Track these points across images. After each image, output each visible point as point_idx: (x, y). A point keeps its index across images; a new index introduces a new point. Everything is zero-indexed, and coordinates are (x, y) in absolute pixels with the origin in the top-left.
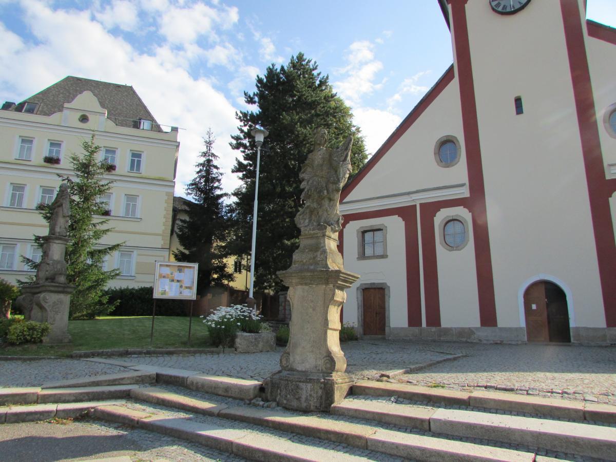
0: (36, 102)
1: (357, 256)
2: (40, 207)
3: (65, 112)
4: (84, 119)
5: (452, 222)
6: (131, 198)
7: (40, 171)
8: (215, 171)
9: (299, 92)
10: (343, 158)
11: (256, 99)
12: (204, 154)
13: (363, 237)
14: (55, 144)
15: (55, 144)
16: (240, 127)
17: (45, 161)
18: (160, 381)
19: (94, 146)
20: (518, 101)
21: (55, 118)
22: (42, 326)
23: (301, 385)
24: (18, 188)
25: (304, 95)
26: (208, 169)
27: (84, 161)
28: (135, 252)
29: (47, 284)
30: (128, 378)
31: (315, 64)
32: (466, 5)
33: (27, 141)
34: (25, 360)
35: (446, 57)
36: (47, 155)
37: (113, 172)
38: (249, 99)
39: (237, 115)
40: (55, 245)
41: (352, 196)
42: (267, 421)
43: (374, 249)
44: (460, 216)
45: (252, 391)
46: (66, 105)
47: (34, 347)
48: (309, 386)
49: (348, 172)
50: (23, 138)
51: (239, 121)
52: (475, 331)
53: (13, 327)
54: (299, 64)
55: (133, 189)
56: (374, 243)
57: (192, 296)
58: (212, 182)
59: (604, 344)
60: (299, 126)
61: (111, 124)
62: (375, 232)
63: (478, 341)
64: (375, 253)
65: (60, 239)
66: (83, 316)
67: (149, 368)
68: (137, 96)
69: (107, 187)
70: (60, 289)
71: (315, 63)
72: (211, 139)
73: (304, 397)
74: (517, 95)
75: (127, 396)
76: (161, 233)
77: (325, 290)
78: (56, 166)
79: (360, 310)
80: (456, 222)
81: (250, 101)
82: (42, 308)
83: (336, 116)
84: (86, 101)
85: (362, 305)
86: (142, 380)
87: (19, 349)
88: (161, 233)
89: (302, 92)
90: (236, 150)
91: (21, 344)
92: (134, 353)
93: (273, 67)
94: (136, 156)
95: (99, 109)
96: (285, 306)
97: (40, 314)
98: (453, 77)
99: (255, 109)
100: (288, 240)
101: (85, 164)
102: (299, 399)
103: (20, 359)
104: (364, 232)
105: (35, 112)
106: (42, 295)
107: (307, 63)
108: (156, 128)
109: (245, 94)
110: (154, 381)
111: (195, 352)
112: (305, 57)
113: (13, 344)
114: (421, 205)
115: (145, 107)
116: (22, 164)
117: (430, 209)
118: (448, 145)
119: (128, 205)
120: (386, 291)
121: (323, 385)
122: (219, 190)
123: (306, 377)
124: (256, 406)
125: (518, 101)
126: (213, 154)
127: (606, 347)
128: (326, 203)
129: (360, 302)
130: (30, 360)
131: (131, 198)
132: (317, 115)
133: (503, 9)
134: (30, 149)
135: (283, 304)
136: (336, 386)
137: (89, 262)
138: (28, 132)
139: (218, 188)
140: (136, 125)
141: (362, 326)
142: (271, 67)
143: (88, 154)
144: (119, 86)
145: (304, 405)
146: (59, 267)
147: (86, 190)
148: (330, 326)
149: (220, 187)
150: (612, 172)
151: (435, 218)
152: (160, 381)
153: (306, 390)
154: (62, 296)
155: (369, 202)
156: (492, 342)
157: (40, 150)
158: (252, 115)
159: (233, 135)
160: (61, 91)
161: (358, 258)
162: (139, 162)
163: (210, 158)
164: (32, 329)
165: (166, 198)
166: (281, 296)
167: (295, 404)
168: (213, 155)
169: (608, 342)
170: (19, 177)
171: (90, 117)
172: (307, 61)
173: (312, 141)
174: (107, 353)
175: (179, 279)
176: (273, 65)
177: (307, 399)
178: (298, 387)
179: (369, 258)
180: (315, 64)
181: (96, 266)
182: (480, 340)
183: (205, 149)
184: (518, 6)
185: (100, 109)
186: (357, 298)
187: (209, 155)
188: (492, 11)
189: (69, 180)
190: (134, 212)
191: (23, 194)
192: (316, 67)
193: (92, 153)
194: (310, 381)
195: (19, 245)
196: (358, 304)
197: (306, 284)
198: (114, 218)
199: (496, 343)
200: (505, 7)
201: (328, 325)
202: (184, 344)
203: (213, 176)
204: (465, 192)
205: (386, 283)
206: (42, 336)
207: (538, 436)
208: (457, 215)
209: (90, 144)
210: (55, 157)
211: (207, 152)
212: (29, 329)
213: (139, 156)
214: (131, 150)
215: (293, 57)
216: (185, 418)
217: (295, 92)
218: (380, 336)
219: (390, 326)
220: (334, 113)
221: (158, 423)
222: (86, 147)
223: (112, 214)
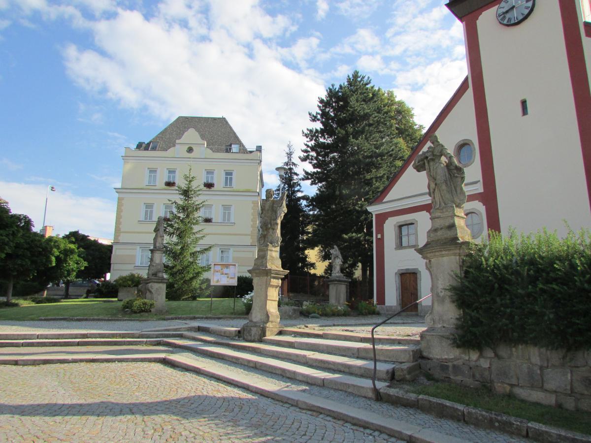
0: (158, 141)
1: (395, 247)
3: (177, 146)
4: (190, 150)
5: (470, 215)
6: (227, 208)
8: (295, 177)
9: (353, 108)
10: (280, 205)
11: (319, 117)
12: (287, 164)
13: (401, 229)
14: (172, 172)
15: (172, 172)
16: (306, 143)
17: (166, 185)
18: (200, 329)
19: (191, 177)
20: (524, 103)
21: (171, 152)
22: (151, 302)
23: (252, 328)
24: (149, 206)
25: (357, 109)
26: (288, 177)
27: (185, 188)
28: (232, 250)
29: (153, 278)
30: (184, 328)
31: (368, 79)
32: (477, 21)
33: (153, 171)
34: (140, 321)
35: (459, 70)
36: (167, 181)
37: (213, 189)
38: (313, 118)
39: (303, 132)
40: (157, 254)
41: (390, 196)
42: (230, 344)
45: (234, 334)
46: (177, 141)
47: (147, 314)
48: (255, 328)
49: (283, 212)
51: (305, 137)
53: (135, 303)
54: (356, 83)
55: (227, 200)
56: (408, 235)
58: (294, 187)
60: (351, 138)
61: (209, 151)
65: (159, 250)
66: (189, 298)
67: (195, 324)
68: (229, 125)
69: (201, 205)
70: (160, 281)
71: (369, 78)
72: (291, 151)
73: (253, 335)
74: (523, 98)
75: (181, 337)
77: (267, 279)
79: (398, 292)
80: (473, 214)
81: (314, 119)
82: (150, 292)
83: (386, 124)
84: (191, 136)
85: (400, 287)
86: (191, 329)
87: (139, 315)
88: (250, 233)
89: (354, 107)
90: (304, 162)
91: (140, 312)
92: (198, 318)
93: (333, 87)
94: (229, 174)
95: (200, 141)
97: (150, 295)
98: (467, 87)
99: (318, 126)
100: (346, 235)
101: (185, 190)
102: (251, 335)
103: (138, 320)
104: (400, 227)
105: (157, 149)
106: (150, 284)
107: (362, 79)
108: (243, 150)
109: (310, 114)
110: (197, 330)
111: (234, 318)
112: (359, 75)
113: (135, 312)
114: (376, 215)
115: (235, 133)
116: (150, 188)
118: (466, 147)
119: (225, 214)
120: (418, 275)
121: (261, 329)
122: (300, 193)
123: (255, 325)
124: (234, 340)
125: (524, 103)
126: (293, 163)
128: (271, 231)
129: (398, 285)
130: (143, 321)
131: (227, 208)
132: (370, 125)
133: (508, 22)
134: (155, 177)
136: (267, 329)
137: (191, 260)
138: (153, 165)
139: (299, 191)
140: (228, 150)
141: (400, 304)
142: (331, 87)
143: (187, 183)
144: (215, 119)
145: (253, 338)
146: (159, 267)
147: (187, 209)
148: (268, 298)
149: (301, 190)
151: (384, 225)
152: (200, 329)
153: (254, 330)
154: (161, 285)
157: (162, 177)
158: (317, 131)
159: (303, 149)
160: (175, 129)
162: (231, 179)
163: (291, 166)
164: (145, 304)
165: (252, 205)
167: (249, 338)
168: (294, 164)
170: (149, 198)
172: (361, 77)
173: (364, 149)
174: (184, 317)
175: (227, 273)
176: (333, 86)
177: (254, 336)
178: (250, 329)
179: (405, 248)
180: (368, 79)
181: (195, 263)
183: (286, 160)
184: (521, 17)
185: (201, 141)
186: (396, 281)
187: (290, 164)
188: (499, 24)
189: (176, 203)
190: (229, 220)
191: (152, 211)
192: (370, 81)
193: (190, 181)
194: (256, 326)
196: (396, 286)
197: (258, 276)
198: (214, 224)
200: (509, 20)
201: (267, 298)
202: (232, 313)
203: (294, 181)
205: (417, 269)
206: (150, 308)
207: (328, 346)
208: (473, 209)
209: (188, 175)
210: (172, 181)
211: (288, 162)
212: (143, 304)
213: (231, 174)
214: (224, 170)
215: (349, 76)
216: (298, 391)
217: (348, 108)
218: (414, 313)
219: (421, 305)
220: (385, 121)
221: (189, 346)
222: (186, 177)
223: (213, 221)
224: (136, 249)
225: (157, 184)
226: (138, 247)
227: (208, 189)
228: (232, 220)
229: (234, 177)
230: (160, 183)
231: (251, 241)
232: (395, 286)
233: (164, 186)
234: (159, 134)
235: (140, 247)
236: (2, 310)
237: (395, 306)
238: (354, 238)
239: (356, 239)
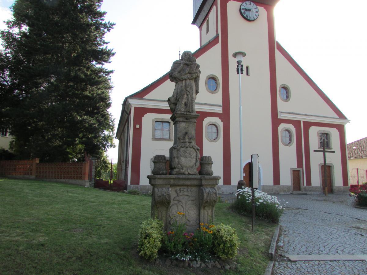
43: (358, 179)
44: (217, 123)
52: (221, 187)
57: (25, 50)
59: (272, 193)
62: (163, 123)
63: (222, 193)
64: (163, 137)
98: (218, 42)
117: (308, 125)
127: (273, 194)
150: (282, 115)
155: (204, 106)
156: (229, 193)
161: (152, 139)
169: (274, 192)
182: (223, 192)
186: (151, 166)
199: (231, 194)
204: (220, 110)
208: (215, 122)
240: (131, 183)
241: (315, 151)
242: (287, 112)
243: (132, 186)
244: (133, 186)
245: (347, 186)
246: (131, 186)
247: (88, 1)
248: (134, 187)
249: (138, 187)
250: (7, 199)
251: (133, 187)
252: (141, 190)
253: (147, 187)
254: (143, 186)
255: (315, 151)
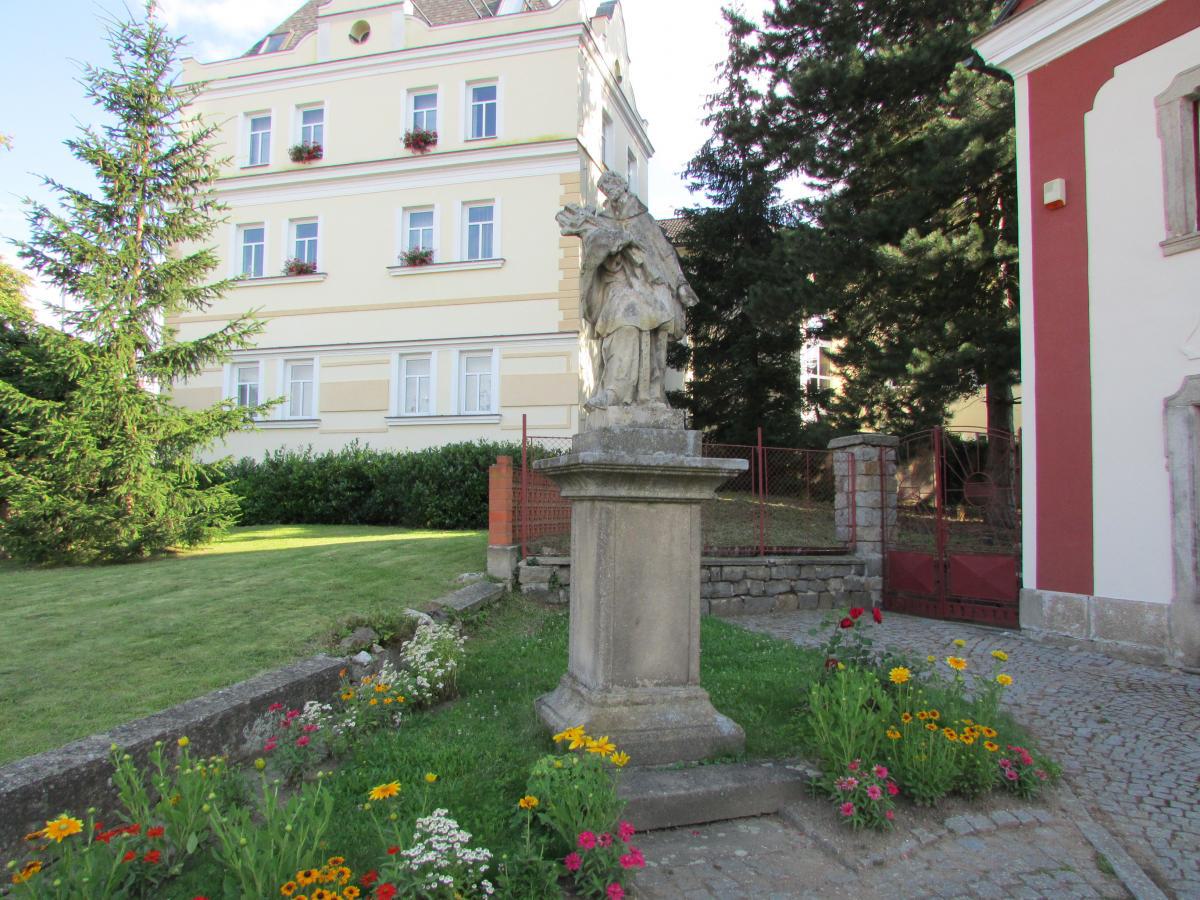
2: (291, 270)
4: (362, 33)
7: (393, 173)
37: (432, 150)
50: (418, 94)
55: (477, 184)
76: (556, 290)
78: (316, 164)
88: (556, 290)
96: (854, 492)
135: (846, 486)
151: (1088, 117)
166: (839, 455)
171: (373, 21)
186: (1169, 454)
190: (488, 251)
191: (491, 225)
195: (435, 352)
196: (1173, 483)
223: (436, 259)
224: (388, 362)
225: (272, 161)
226: (394, 356)
227: (419, 153)
228: (496, 254)
229: (500, 101)
230: (279, 156)
231: (560, 315)
232: (1165, 477)
233: (287, 162)
234: (298, 12)
235: (402, 355)
236: (5, 577)
237: (1158, 608)
238: (931, 254)
239: (943, 258)
240: (1043, 582)
241: (524, 416)
242: (584, 146)
243: (1048, 595)
244: (1056, 601)
245: (1083, 597)
246: (1040, 597)
247: (429, 896)
248: (1060, 607)
249: (1081, 610)
250: (885, 337)
251: (1052, 609)
252: (1104, 634)
253: (1151, 618)
254: (1118, 605)
255: (524, 416)
